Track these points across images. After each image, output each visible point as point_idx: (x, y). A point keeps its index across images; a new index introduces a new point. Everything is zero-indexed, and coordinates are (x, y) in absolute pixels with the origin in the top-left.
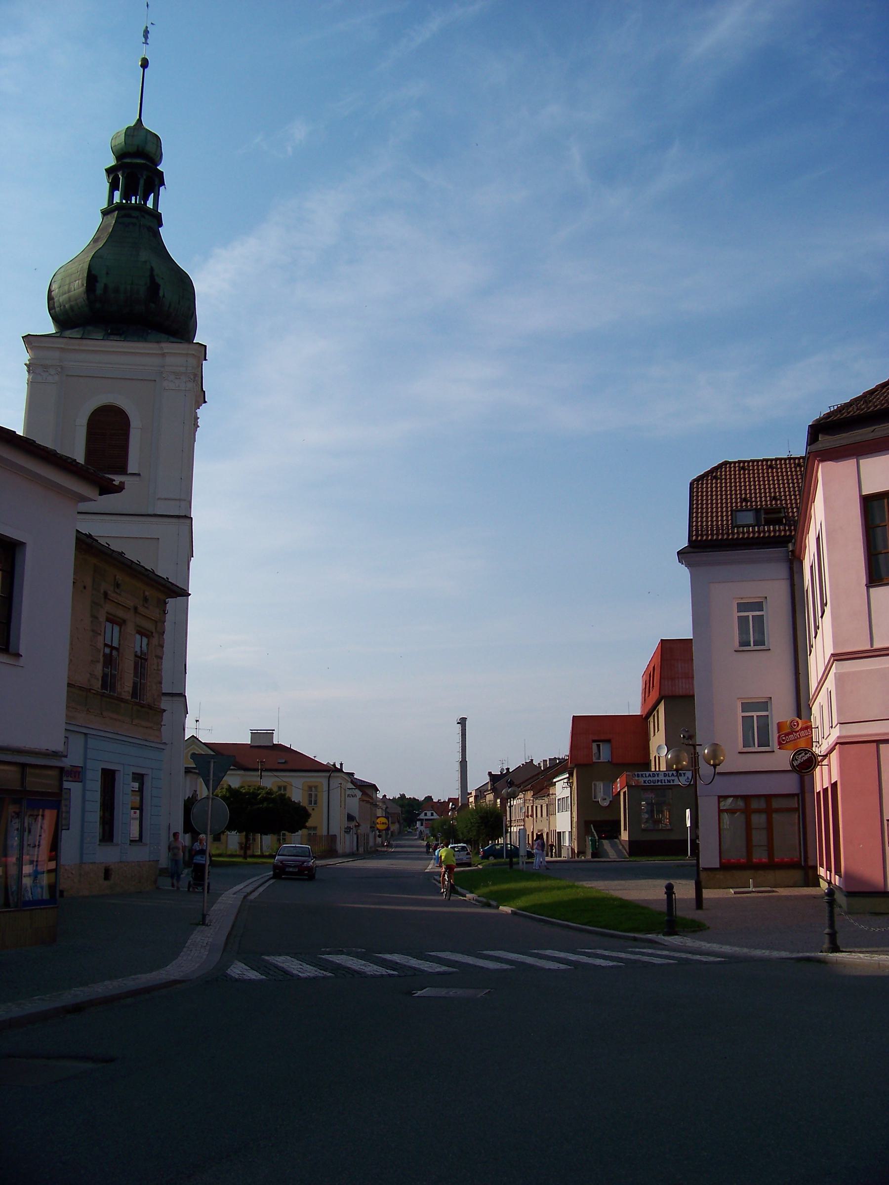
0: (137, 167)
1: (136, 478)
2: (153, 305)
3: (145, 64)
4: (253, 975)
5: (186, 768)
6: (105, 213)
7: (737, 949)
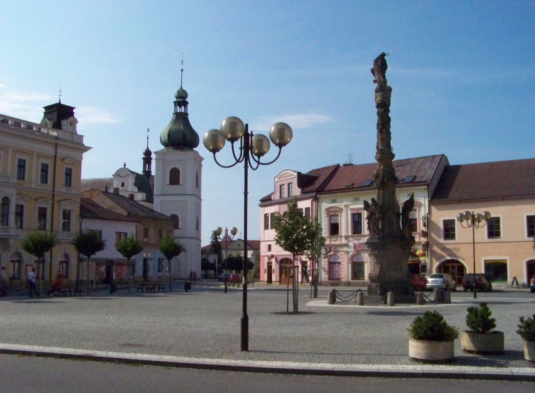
0: (182, 99)
3: (182, 70)
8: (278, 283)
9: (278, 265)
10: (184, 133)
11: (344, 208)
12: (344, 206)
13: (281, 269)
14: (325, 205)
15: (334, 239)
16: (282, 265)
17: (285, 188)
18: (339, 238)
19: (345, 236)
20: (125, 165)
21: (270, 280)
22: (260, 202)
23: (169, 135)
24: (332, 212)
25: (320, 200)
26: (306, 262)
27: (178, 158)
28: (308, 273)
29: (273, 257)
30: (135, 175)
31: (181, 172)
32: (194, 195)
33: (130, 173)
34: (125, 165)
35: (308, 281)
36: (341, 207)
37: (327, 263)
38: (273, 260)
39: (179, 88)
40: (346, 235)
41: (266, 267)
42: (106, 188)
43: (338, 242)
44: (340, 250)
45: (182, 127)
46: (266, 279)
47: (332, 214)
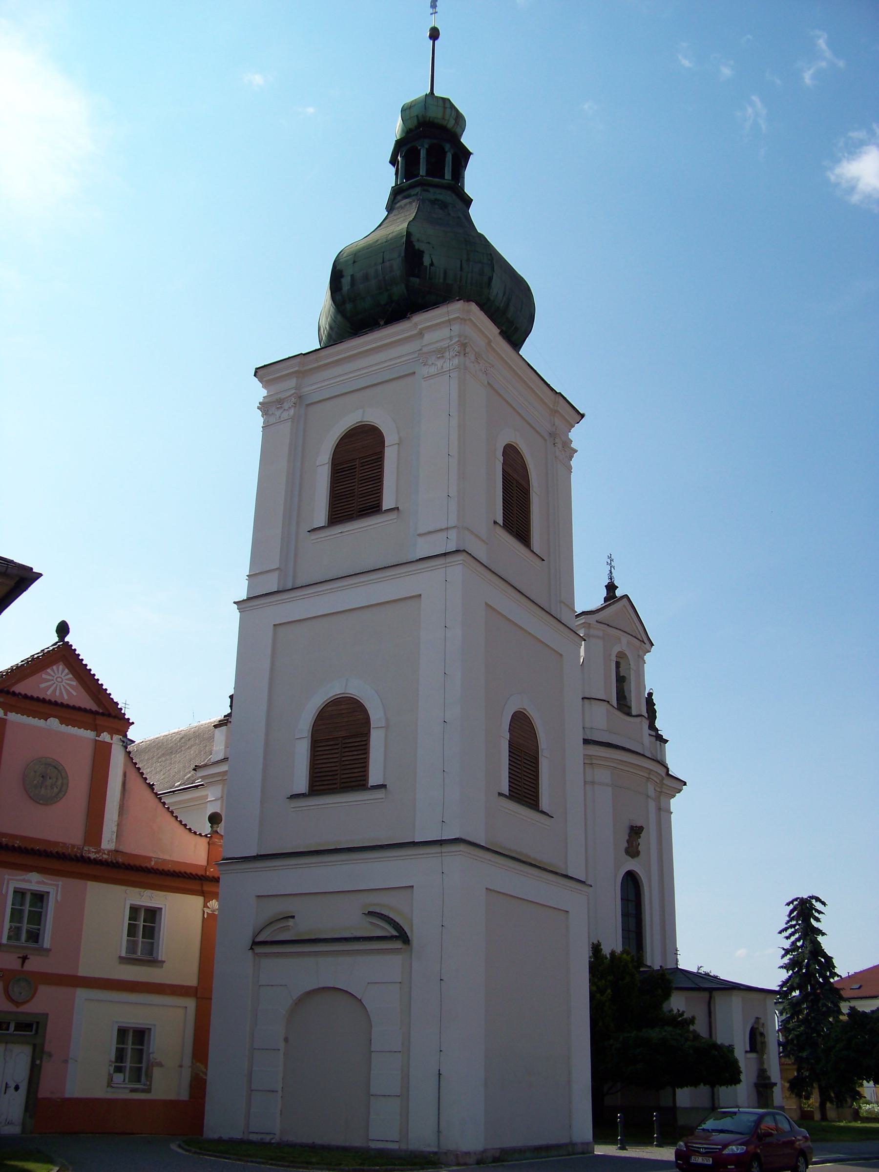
2: (415, 280)
3: (434, 34)
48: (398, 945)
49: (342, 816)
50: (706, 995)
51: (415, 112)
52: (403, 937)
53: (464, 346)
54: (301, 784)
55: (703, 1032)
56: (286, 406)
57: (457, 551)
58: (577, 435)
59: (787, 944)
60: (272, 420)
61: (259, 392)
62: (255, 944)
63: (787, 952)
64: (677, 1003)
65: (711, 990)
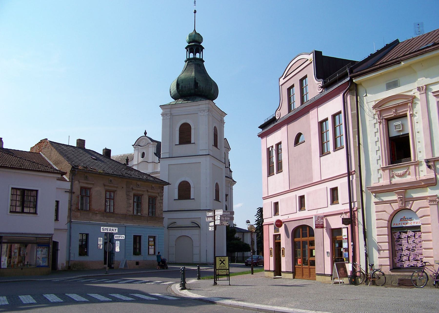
0: (195, 45)
1: (194, 144)
2: (196, 90)
3: (195, 12)
4: (91, 295)
5: (140, 237)
6: (186, 62)
7: (220, 290)
8: (291, 276)
9: (290, 239)
10: (195, 81)
11: (417, 94)
12: (419, 89)
13: (295, 246)
14: (370, 99)
15: (401, 172)
16: (296, 239)
17: (296, 91)
18: (412, 168)
19: (427, 161)
20: (145, 133)
21: (278, 271)
22: (261, 130)
23: (178, 85)
24: (389, 109)
25: (361, 90)
26: (339, 230)
27: (195, 113)
28: (345, 253)
29: (280, 226)
30: (157, 143)
31: (192, 127)
32: (208, 155)
33: (150, 141)
34: (145, 133)
35: (344, 274)
36: (411, 94)
37: (385, 231)
38: (282, 230)
39: (192, 31)
40: (430, 157)
41: (272, 245)
42: (127, 160)
43: (410, 178)
44: (415, 195)
45: (193, 74)
46: (272, 268)
47: (391, 114)
48: (198, 228)
49: (185, 204)
50: (242, 233)
51: (192, 38)
52: (199, 227)
53: (209, 110)
54: (177, 197)
55: (242, 240)
56: (168, 115)
57: (208, 155)
58: (225, 119)
59: (257, 219)
60: (165, 118)
61: (161, 111)
62: (168, 228)
63: (257, 221)
64: (237, 235)
65: (243, 232)
